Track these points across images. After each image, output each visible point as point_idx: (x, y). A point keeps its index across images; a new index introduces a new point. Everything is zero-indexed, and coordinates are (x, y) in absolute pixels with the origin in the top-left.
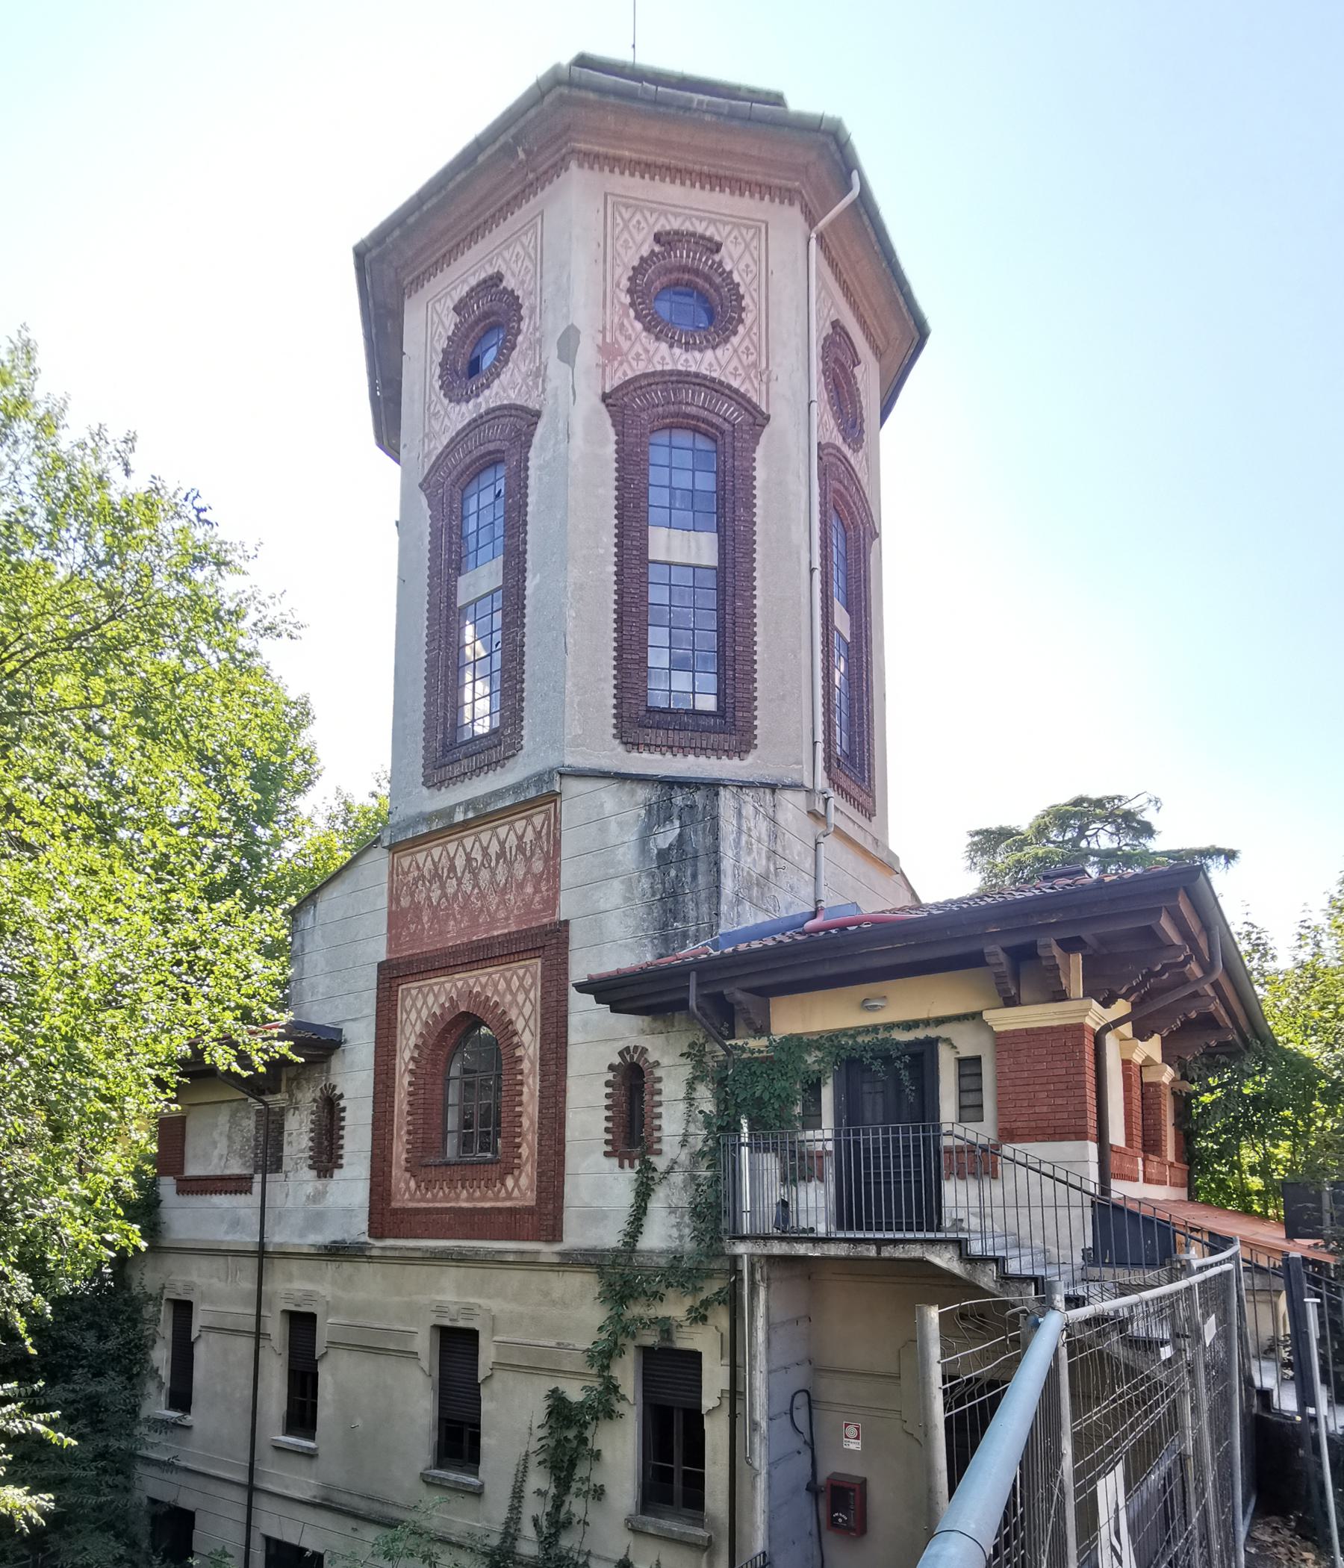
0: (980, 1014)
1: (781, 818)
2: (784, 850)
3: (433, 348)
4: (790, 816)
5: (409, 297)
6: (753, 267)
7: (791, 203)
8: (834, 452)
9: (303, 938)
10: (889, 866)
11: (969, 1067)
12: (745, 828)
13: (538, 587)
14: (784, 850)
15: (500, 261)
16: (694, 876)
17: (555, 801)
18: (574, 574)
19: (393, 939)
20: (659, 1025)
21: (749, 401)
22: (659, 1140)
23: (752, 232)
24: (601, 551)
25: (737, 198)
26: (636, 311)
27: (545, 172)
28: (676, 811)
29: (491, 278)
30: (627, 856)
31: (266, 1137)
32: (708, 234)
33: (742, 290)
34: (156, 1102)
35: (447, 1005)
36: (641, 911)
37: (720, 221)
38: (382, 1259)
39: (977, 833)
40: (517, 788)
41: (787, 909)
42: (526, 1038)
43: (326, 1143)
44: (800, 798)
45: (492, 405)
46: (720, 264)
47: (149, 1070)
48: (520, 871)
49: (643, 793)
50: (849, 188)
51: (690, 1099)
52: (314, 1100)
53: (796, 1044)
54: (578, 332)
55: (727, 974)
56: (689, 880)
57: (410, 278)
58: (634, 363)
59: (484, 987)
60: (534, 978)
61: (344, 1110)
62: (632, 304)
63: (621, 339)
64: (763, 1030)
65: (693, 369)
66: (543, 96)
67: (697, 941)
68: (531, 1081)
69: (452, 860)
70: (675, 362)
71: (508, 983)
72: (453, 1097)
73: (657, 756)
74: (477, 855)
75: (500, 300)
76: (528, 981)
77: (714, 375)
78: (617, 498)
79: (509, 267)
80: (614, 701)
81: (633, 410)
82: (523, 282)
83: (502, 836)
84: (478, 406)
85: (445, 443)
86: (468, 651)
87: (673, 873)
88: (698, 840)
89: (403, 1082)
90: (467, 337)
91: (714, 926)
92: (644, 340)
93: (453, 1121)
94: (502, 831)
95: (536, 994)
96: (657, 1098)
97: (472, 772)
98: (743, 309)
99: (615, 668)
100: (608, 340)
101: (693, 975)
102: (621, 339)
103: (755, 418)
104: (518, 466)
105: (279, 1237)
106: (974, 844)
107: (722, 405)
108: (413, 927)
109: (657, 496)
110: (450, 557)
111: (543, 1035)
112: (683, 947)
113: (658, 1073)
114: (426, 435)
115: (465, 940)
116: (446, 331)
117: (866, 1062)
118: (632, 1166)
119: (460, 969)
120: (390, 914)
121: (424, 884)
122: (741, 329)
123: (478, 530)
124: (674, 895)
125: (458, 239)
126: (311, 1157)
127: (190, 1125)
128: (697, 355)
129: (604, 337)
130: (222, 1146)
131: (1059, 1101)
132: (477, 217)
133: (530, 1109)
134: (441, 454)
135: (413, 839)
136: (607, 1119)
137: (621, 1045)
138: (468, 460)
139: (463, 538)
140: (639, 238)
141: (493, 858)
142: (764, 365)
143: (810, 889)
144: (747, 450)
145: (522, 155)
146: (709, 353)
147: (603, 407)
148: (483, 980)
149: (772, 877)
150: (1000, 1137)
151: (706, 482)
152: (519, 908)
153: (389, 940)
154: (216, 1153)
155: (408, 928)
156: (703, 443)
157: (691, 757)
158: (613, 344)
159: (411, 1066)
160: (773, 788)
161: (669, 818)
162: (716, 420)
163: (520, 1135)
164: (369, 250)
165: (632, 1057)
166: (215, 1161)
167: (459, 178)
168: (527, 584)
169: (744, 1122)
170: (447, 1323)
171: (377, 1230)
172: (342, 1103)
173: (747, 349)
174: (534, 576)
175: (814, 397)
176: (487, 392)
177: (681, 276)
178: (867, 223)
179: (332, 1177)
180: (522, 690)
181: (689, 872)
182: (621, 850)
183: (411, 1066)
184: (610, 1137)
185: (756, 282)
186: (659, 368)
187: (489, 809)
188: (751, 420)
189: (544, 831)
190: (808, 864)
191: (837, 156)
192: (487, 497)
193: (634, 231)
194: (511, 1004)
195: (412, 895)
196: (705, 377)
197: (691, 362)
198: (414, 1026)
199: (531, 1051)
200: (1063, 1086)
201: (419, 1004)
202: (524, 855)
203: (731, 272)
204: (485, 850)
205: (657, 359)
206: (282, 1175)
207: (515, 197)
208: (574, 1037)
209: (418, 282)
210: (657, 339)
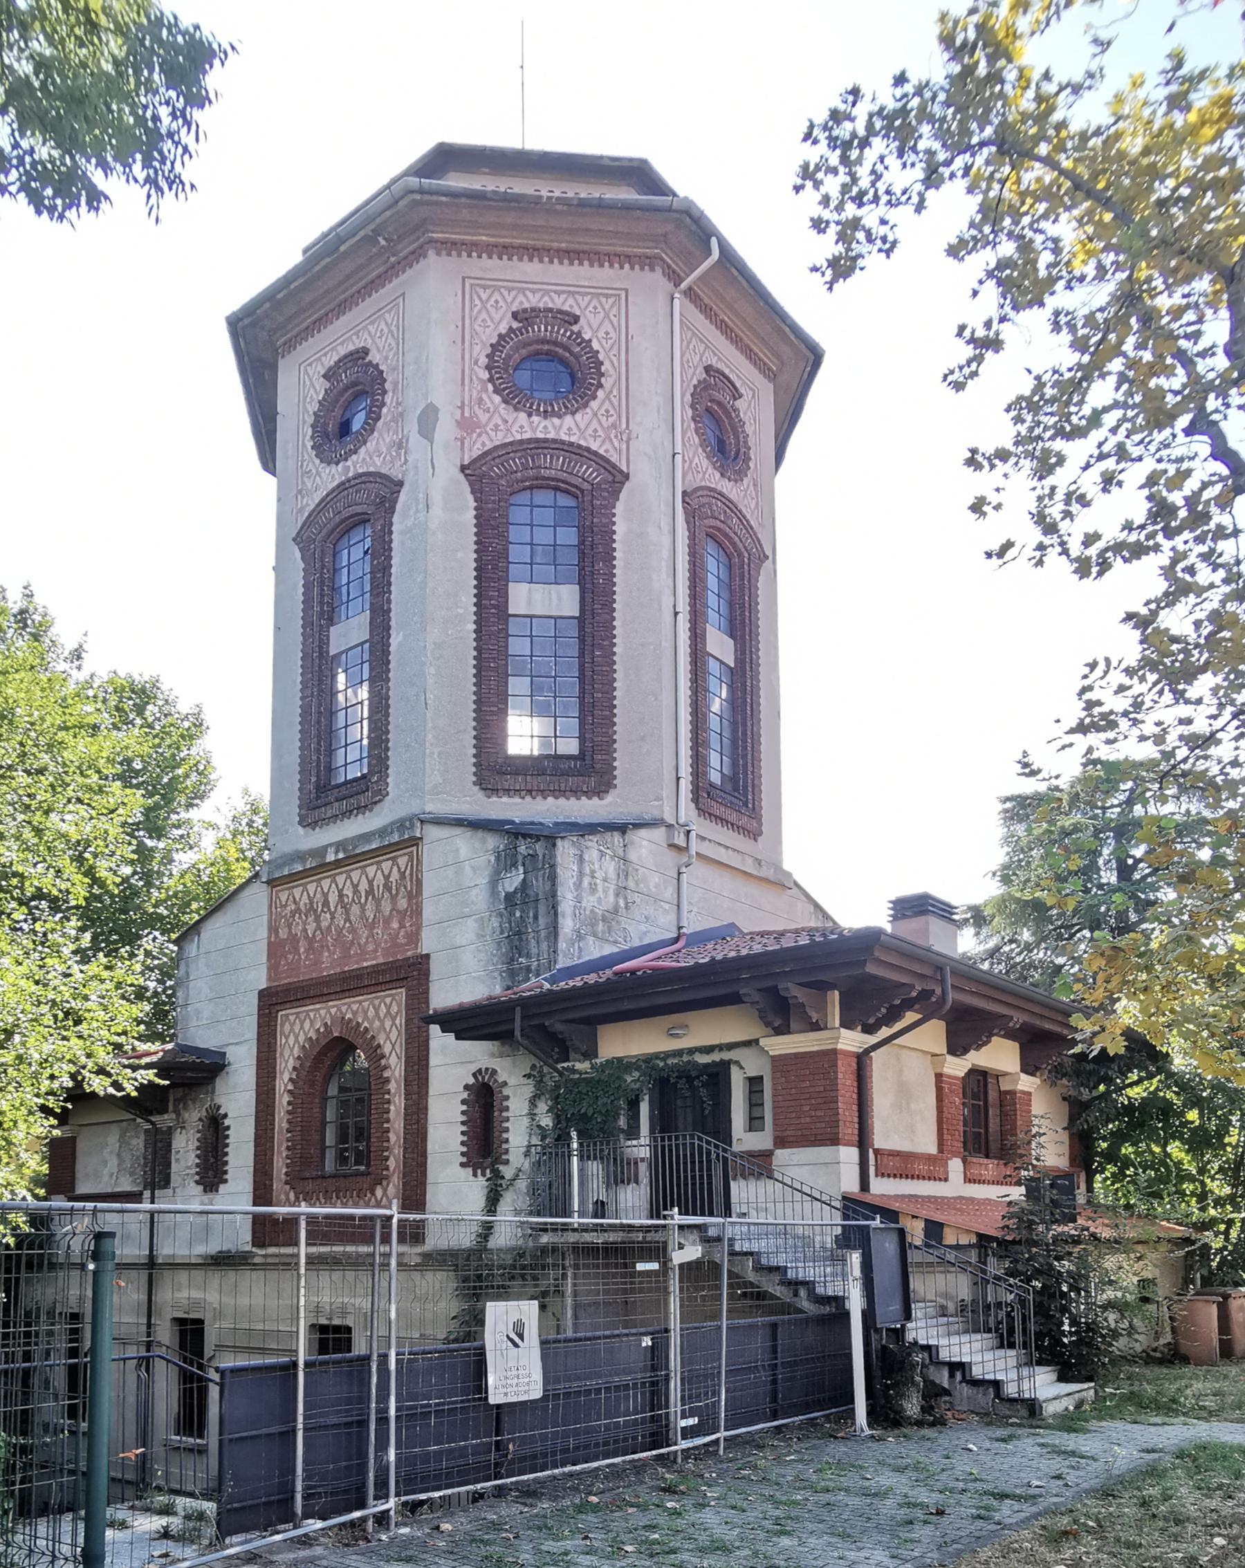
0: (757, 1041)
1: (632, 855)
2: (637, 884)
3: (305, 408)
4: (644, 852)
5: (283, 357)
6: (613, 334)
7: (652, 269)
8: (705, 493)
9: (187, 965)
10: (782, 883)
11: (754, 1083)
12: (587, 871)
13: (400, 644)
14: (637, 884)
15: (366, 335)
16: (536, 918)
17: (417, 845)
18: (434, 633)
19: (273, 968)
20: (507, 1049)
21: (608, 461)
22: (507, 1152)
23: (611, 300)
24: (461, 611)
25: (596, 268)
26: (494, 385)
27: (406, 258)
28: (520, 858)
29: (357, 351)
30: (479, 897)
31: (155, 1153)
32: (566, 308)
33: (601, 357)
34: (43, 1127)
35: (322, 1030)
36: (492, 948)
37: (578, 293)
38: (264, 1266)
39: (1008, 799)
40: (382, 832)
41: (641, 939)
42: (393, 1061)
43: (212, 1160)
44: (659, 834)
45: (360, 471)
46: (579, 334)
47: (36, 1100)
48: (386, 907)
49: (493, 842)
50: (709, 253)
51: (532, 1115)
52: (200, 1120)
53: (621, 1065)
54: (436, 410)
55: (545, 1009)
56: (531, 920)
57: (283, 339)
58: (493, 434)
59: (355, 1013)
60: (399, 1005)
61: (228, 1128)
62: (491, 380)
63: (479, 412)
64: (591, 1053)
65: (551, 435)
66: (397, 202)
67: (538, 975)
68: (397, 1099)
69: (325, 895)
70: (534, 430)
71: (377, 1010)
72: (330, 1115)
73: (517, 800)
74: (348, 892)
75: (366, 372)
76: (394, 1009)
77: (573, 439)
78: (476, 560)
79: (374, 342)
80: (474, 751)
81: (492, 478)
82: (386, 358)
83: (371, 875)
84: (347, 469)
85: (317, 501)
86: (341, 697)
87: (518, 914)
88: (539, 886)
89: (282, 1101)
90: (337, 401)
91: (552, 961)
92: (502, 412)
93: (330, 1139)
94: (371, 870)
95: (400, 1021)
96: (505, 1114)
97: (343, 814)
98: (603, 375)
99: (475, 719)
100: (467, 414)
101: (518, 1009)
102: (479, 412)
103: (614, 476)
104: (383, 530)
105: (165, 1251)
106: (1006, 811)
107: (581, 467)
108: (290, 957)
109: (518, 553)
110: (322, 608)
111: (407, 1058)
112: (528, 979)
113: (506, 1092)
114: (300, 492)
115: (338, 970)
116: (317, 394)
117: (672, 1080)
118: (484, 1175)
119: (333, 997)
120: (270, 943)
121: (300, 917)
122: (600, 393)
123: (348, 583)
124: (519, 933)
125: (328, 308)
126: (197, 1173)
127: (81, 1146)
128: (556, 421)
129: (463, 413)
130: (113, 1163)
131: (819, 1113)
132: (344, 292)
133: (396, 1126)
134: (313, 511)
135: (290, 875)
136: (463, 1133)
137: (474, 1068)
138: (337, 519)
139: (335, 589)
140: (497, 317)
141: (363, 894)
142: (624, 426)
143: (672, 917)
144: (605, 507)
145: (383, 242)
146: (568, 419)
147: (462, 477)
148: (355, 1007)
149: (622, 911)
150: (775, 1144)
151: (569, 536)
152: (386, 942)
153: (269, 969)
154: (106, 1171)
155: (286, 958)
156: (564, 501)
157: (550, 799)
158: (471, 417)
159: (290, 1087)
160: (622, 829)
161: (514, 865)
162: (573, 480)
163: (387, 1149)
164: (241, 319)
165: (483, 1078)
166: (106, 1178)
167: (323, 263)
168: (391, 640)
169: (574, 1134)
170: (323, 1321)
171: (258, 1241)
172: (227, 1122)
173: (607, 411)
174: (398, 634)
175: (679, 449)
176: (354, 457)
177: (540, 347)
178: (736, 273)
179: (217, 1191)
180: (388, 740)
181: (531, 914)
182: (474, 892)
183: (290, 1087)
184: (464, 1149)
185: (616, 348)
186: (519, 437)
187: (358, 851)
188: (610, 478)
189: (408, 872)
190: (669, 893)
191: (694, 227)
192: (357, 553)
193: (492, 311)
194: (379, 1029)
195: (290, 927)
196: (563, 442)
197: (550, 428)
198: (292, 1049)
199: (397, 1073)
200: (820, 1101)
201: (297, 1029)
202: (390, 893)
203: (590, 341)
204: (355, 887)
205: (516, 428)
206: (171, 1191)
207: (379, 277)
208: (434, 1060)
209: (290, 345)
210: (516, 409)
